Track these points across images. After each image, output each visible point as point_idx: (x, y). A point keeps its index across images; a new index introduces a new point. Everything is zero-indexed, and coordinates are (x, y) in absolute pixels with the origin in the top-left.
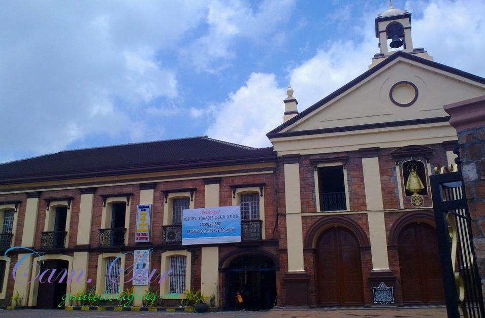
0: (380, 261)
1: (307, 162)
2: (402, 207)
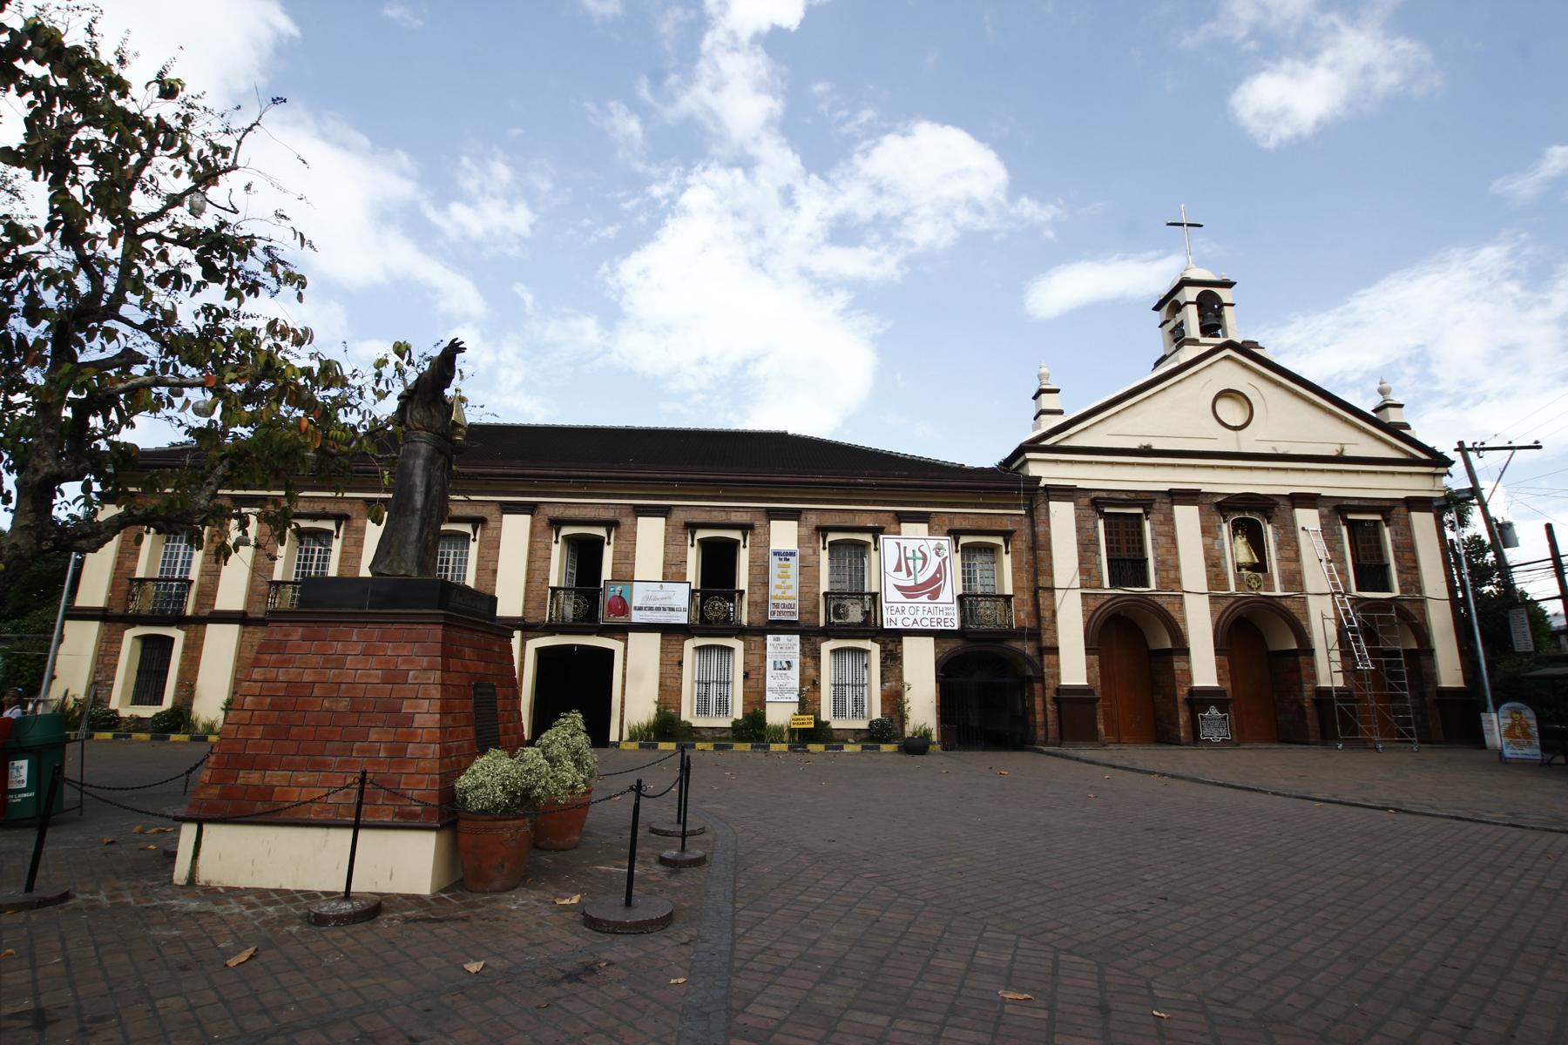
0: (1204, 670)
1: (1085, 501)
2: (1233, 589)
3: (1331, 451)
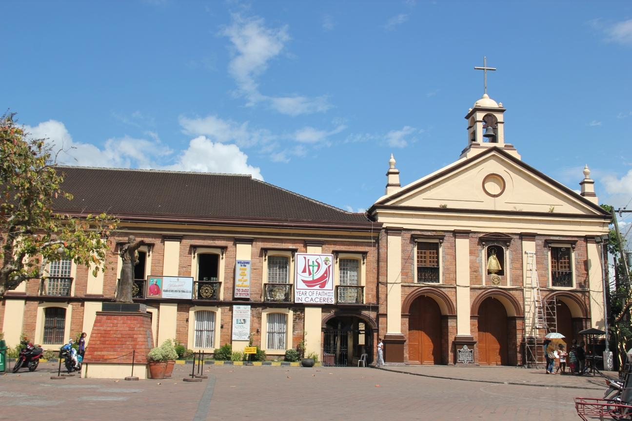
3: (546, 210)
